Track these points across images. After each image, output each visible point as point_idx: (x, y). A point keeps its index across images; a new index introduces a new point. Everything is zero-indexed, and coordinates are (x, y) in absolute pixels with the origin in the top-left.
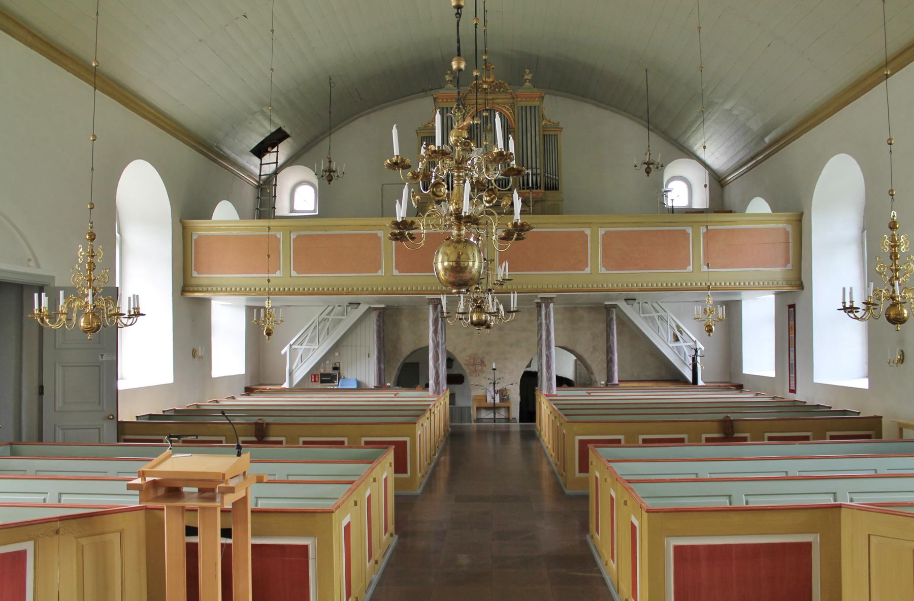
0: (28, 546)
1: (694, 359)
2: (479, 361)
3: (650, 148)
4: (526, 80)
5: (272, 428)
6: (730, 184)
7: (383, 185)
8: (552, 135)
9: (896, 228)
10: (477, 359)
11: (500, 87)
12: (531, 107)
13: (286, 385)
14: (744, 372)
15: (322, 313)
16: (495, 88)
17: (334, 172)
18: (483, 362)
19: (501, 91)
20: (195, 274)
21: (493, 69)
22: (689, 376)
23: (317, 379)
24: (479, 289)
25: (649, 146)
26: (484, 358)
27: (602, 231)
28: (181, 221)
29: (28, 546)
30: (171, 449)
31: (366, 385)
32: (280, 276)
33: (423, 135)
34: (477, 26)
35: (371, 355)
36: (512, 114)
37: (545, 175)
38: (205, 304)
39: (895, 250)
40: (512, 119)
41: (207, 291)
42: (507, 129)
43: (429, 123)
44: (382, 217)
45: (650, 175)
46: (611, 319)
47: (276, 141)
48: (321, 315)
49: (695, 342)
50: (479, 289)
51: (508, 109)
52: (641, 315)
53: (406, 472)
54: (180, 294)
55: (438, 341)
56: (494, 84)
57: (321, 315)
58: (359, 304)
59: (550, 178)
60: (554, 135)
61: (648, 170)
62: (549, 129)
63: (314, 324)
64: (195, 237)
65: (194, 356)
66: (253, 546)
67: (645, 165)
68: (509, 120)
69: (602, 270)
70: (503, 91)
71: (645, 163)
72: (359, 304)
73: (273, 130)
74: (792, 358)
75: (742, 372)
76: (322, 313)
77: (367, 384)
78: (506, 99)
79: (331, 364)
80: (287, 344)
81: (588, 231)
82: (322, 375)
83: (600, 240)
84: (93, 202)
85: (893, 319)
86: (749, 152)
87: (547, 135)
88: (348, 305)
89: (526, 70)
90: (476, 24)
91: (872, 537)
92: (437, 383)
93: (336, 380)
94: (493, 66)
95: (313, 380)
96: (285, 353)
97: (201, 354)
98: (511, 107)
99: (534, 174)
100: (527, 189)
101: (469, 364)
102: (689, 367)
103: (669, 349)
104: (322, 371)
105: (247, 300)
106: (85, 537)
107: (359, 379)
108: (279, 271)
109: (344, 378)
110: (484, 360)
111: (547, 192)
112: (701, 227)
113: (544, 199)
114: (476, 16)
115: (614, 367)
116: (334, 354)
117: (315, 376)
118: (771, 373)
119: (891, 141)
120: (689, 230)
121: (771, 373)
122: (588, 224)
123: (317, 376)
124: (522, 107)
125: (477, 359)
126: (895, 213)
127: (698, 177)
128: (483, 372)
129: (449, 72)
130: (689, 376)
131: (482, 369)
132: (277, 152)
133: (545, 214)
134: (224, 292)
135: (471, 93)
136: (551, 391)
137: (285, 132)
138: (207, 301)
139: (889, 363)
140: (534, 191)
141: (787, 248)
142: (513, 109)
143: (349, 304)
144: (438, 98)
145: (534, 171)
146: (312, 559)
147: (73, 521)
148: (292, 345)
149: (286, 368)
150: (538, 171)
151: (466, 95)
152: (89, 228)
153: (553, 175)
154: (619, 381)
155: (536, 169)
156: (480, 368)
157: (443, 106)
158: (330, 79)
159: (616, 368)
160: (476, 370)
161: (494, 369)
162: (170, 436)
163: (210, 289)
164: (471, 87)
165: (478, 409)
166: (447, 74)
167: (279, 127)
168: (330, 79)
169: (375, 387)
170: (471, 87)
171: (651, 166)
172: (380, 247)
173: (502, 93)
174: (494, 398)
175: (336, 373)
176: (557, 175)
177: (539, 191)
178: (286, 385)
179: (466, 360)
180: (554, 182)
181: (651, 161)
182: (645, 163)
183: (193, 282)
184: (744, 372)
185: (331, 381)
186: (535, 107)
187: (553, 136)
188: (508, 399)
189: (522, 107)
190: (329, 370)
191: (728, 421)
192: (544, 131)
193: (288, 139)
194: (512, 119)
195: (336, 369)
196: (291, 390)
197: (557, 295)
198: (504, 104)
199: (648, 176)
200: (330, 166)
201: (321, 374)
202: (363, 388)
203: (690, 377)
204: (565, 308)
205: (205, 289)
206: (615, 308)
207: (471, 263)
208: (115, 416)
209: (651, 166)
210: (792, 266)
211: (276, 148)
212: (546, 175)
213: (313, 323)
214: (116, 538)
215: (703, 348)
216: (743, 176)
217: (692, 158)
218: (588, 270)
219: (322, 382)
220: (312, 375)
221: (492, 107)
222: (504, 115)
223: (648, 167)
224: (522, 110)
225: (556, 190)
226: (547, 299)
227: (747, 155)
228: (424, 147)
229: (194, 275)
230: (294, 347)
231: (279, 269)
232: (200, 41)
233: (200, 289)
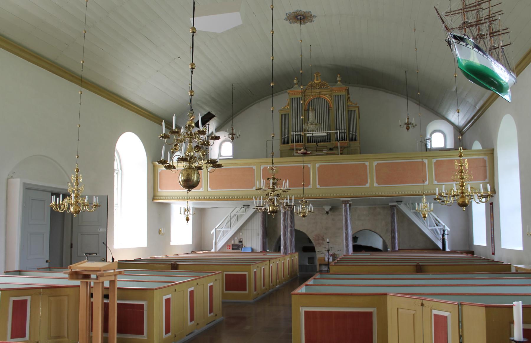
0: (28, 298)
1: (443, 235)
3: (409, 115)
4: (338, 81)
5: (180, 266)
6: (466, 133)
7: (267, 141)
8: (353, 110)
9: (462, 156)
11: (324, 85)
12: (341, 96)
13: (213, 250)
15: (233, 211)
16: (321, 86)
17: (235, 135)
18: (323, 239)
19: (324, 87)
20: (159, 190)
21: (320, 75)
22: (440, 246)
23: (230, 247)
24: (272, 194)
25: (408, 114)
27: (375, 163)
28: (152, 163)
29: (28, 298)
30: (87, 260)
31: (256, 250)
32: (202, 191)
33: (282, 113)
34: (273, 60)
35: (259, 235)
36: (331, 100)
37: (349, 133)
38: (166, 206)
39: (462, 168)
40: (331, 102)
41: (170, 199)
42: (328, 108)
43: (285, 107)
44: (267, 158)
45: (409, 130)
46: (394, 213)
47: (208, 119)
48: (232, 212)
49: (444, 226)
50: (272, 194)
51: (328, 97)
52: (411, 211)
53: (246, 290)
54: (152, 200)
55: (286, 225)
56: (321, 83)
57: (232, 212)
58: (249, 206)
59: (353, 134)
60: (355, 110)
61: (407, 128)
62: (352, 107)
63: (228, 218)
64: (159, 171)
65: (159, 233)
66: (118, 304)
67: (406, 125)
68: (329, 104)
69: (376, 185)
70: (326, 87)
71: (406, 124)
72: (249, 206)
73: (206, 113)
74: (492, 234)
76: (233, 211)
77: (257, 249)
78: (328, 91)
79: (238, 239)
80: (214, 229)
81: (367, 163)
82: (233, 245)
83: (374, 168)
84: (78, 155)
85: (461, 205)
86: (471, 114)
87: (350, 110)
88: (243, 207)
90: (272, 60)
91: (399, 309)
92: (285, 248)
93: (240, 248)
94: (320, 74)
95: (228, 248)
96: (213, 233)
97: (163, 232)
98: (330, 96)
99: (341, 133)
100: (337, 141)
102: (440, 241)
103: (428, 231)
104: (233, 242)
105: (194, 204)
106: (52, 296)
107: (253, 247)
108: (202, 188)
109: (245, 247)
111: (351, 142)
112: (433, 159)
113: (349, 146)
114: (272, 55)
115: (395, 241)
116: (240, 234)
117: (229, 246)
118: (485, 244)
119: (459, 111)
120: (426, 161)
121: (485, 244)
122: (367, 159)
123: (230, 246)
124: (336, 96)
126: (461, 148)
127: (449, 130)
128: (323, 244)
129: (296, 79)
130: (440, 246)
132: (209, 125)
133: (349, 154)
134: (181, 199)
135: (308, 89)
136: (348, 253)
137: (212, 114)
138: (167, 205)
139: (528, 234)
140: (341, 142)
141: (485, 170)
142: (331, 97)
143: (243, 206)
144: (290, 93)
145: (343, 131)
146: (145, 311)
147: (47, 289)
148: (217, 228)
149: (213, 241)
150: (345, 131)
151: (305, 91)
152: (76, 167)
153: (351, 132)
154: (399, 249)
155: (344, 129)
157: (292, 97)
158: (232, 85)
159: (397, 241)
160: (319, 243)
161: (328, 242)
162: (86, 254)
163: (167, 198)
164: (308, 86)
165: (320, 265)
166: (295, 80)
167: (208, 112)
168: (232, 85)
169: (260, 251)
170: (308, 86)
171: (410, 125)
172: (254, 174)
173: (325, 88)
174: (329, 259)
175: (240, 244)
176: (356, 132)
177: (346, 141)
178: (213, 250)
179: (314, 237)
180: (315, 139)
181: (409, 123)
182: (406, 124)
183: (159, 194)
185: (238, 249)
186: (343, 95)
187: (354, 111)
189: (336, 96)
190: (237, 242)
191: (418, 265)
192: (348, 108)
193: (215, 118)
194: (331, 102)
195: (240, 242)
196: (215, 252)
197: (351, 199)
198: (327, 95)
199: (408, 131)
200: (233, 132)
201: (232, 245)
202: (255, 252)
203: (441, 247)
204: (370, 208)
205: (164, 198)
206: (396, 207)
207: (193, 178)
208: (105, 259)
209: (410, 125)
210: (489, 180)
211: (208, 123)
212: (350, 132)
213: (228, 216)
214: (66, 298)
215: (449, 230)
216: (470, 129)
217: (444, 119)
218: (368, 185)
219: (233, 249)
220: (227, 245)
221: (320, 96)
222: (326, 101)
223: (408, 126)
224: (343, 97)
225: (356, 141)
226: (346, 201)
227: (470, 116)
229: (159, 191)
230: (217, 229)
231: (202, 187)
232: (157, 71)
233: (162, 198)
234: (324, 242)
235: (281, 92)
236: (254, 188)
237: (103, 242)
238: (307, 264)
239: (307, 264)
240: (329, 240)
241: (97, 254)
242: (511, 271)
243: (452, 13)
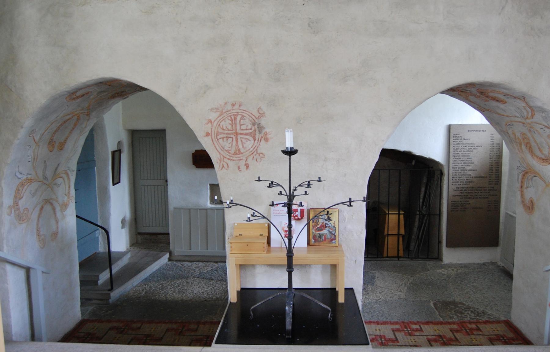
2: (248, 123)
10: (243, 117)
14: (339, 302)
18: (260, 128)
26: (262, 115)
75: (338, 301)
89: (286, 337)
101: (218, 134)
110: (263, 122)
125: (243, 117)
128: (257, 155)
131: (256, 148)
156: (249, 144)
160: (238, 152)
161: (290, 152)
184: (339, 302)
188: (333, 238)
228: (293, 219)
234: (263, 147)
235: (374, 259)
236: (464, 315)
237: (28, 161)
238: (209, 205)
239: (209, 205)
240: (295, 138)
241: (29, 160)
242: (449, 245)
243: (470, 145)
